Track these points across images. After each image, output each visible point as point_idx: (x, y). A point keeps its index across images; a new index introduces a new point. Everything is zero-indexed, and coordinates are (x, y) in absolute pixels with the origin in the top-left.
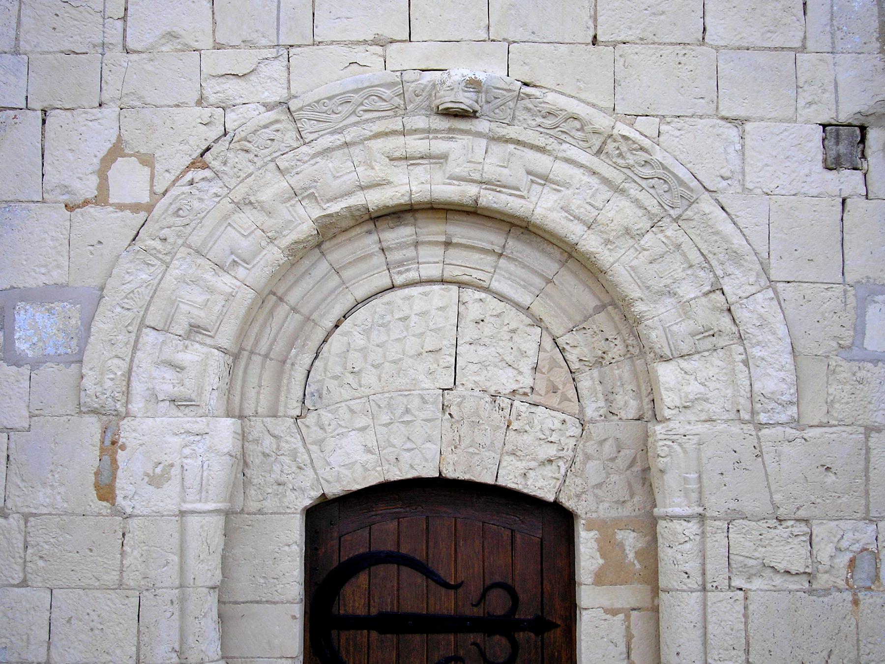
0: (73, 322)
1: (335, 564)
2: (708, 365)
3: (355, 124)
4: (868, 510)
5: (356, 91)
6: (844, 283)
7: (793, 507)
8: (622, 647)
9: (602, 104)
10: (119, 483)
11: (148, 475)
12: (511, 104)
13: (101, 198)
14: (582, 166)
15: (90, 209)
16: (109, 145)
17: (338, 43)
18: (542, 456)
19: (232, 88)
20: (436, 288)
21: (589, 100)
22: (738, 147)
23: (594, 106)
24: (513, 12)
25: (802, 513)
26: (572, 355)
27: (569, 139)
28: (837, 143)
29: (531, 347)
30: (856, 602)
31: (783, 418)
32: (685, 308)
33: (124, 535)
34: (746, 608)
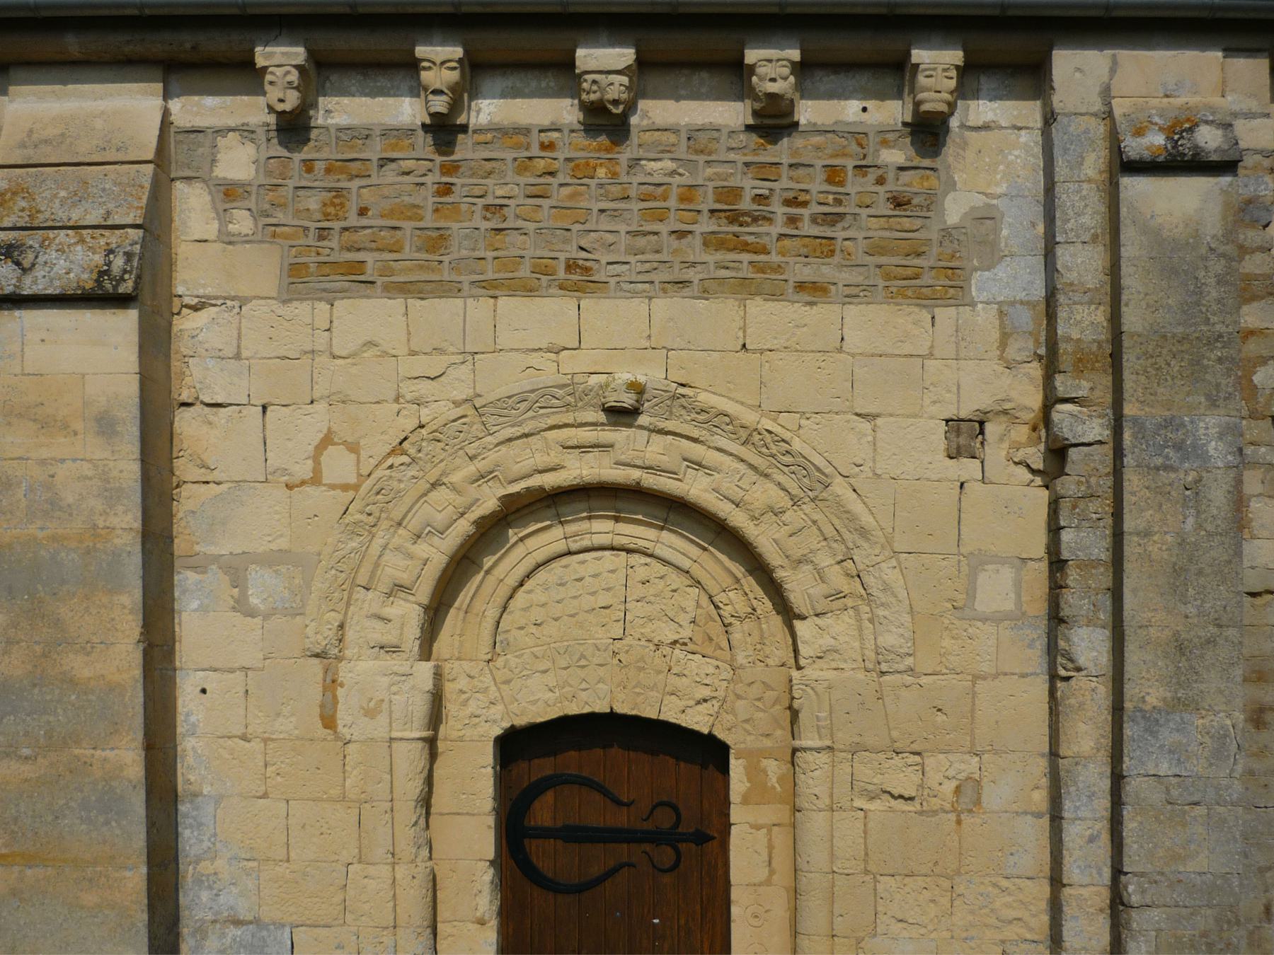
0: (297, 581)
1: (525, 784)
2: (839, 622)
3: (533, 418)
4: (973, 744)
5: (533, 391)
6: (960, 554)
7: (908, 742)
8: (765, 857)
9: (750, 402)
10: (339, 715)
11: (363, 709)
12: (668, 402)
13: (316, 480)
14: (731, 454)
15: (307, 489)
16: (321, 435)
17: (517, 350)
18: (699, 696)
19: (424, 387)
20: (607, 553)
21: (738, 399)
22: (870, 438)
23: (742, 403)
24: (671, 324)
25: (915, 747)
26: (726, 611)
27: (719, 431)
28: (958, 436)
29: (690, 605)
30: (959, 822)
31: (901, 667)
32: (821, 576)
33: (345, 757)
34: (865, 825)
